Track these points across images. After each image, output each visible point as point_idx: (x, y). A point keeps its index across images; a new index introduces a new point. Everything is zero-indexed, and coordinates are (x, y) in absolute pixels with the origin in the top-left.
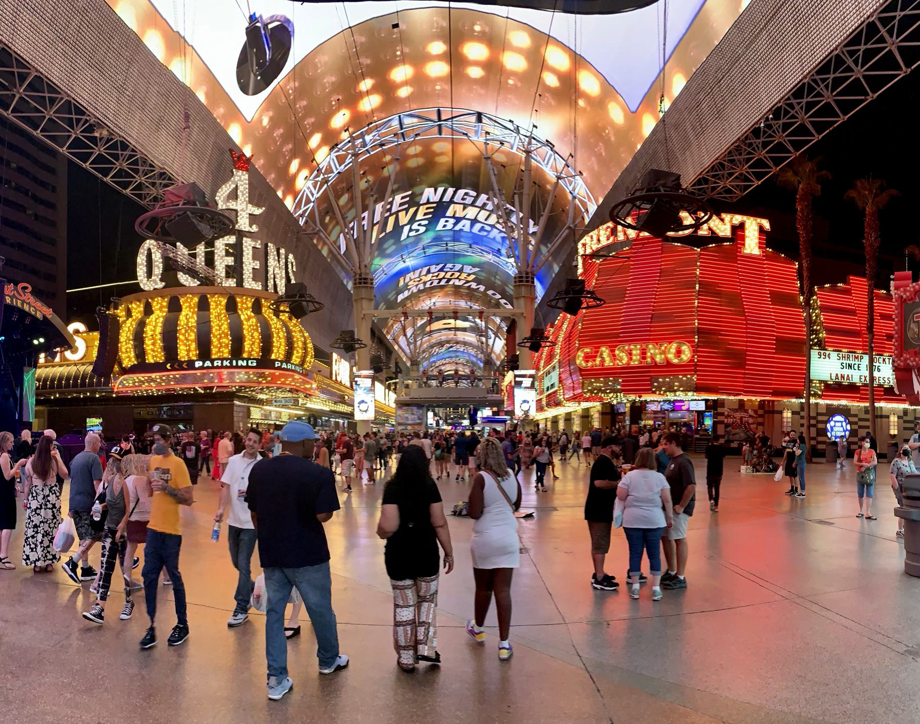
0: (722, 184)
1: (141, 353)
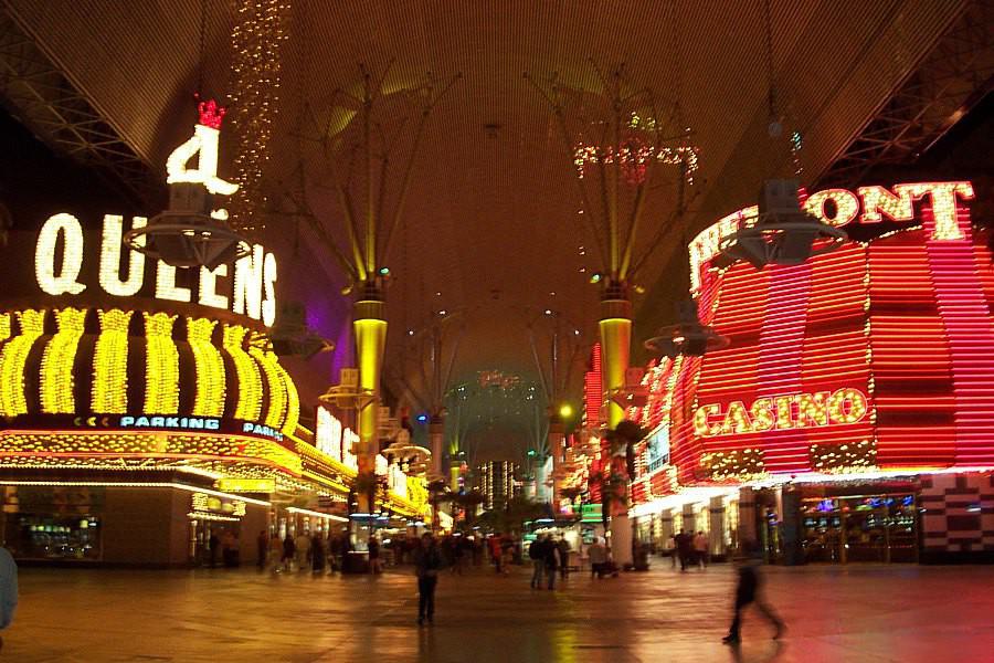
0: (888, 144)
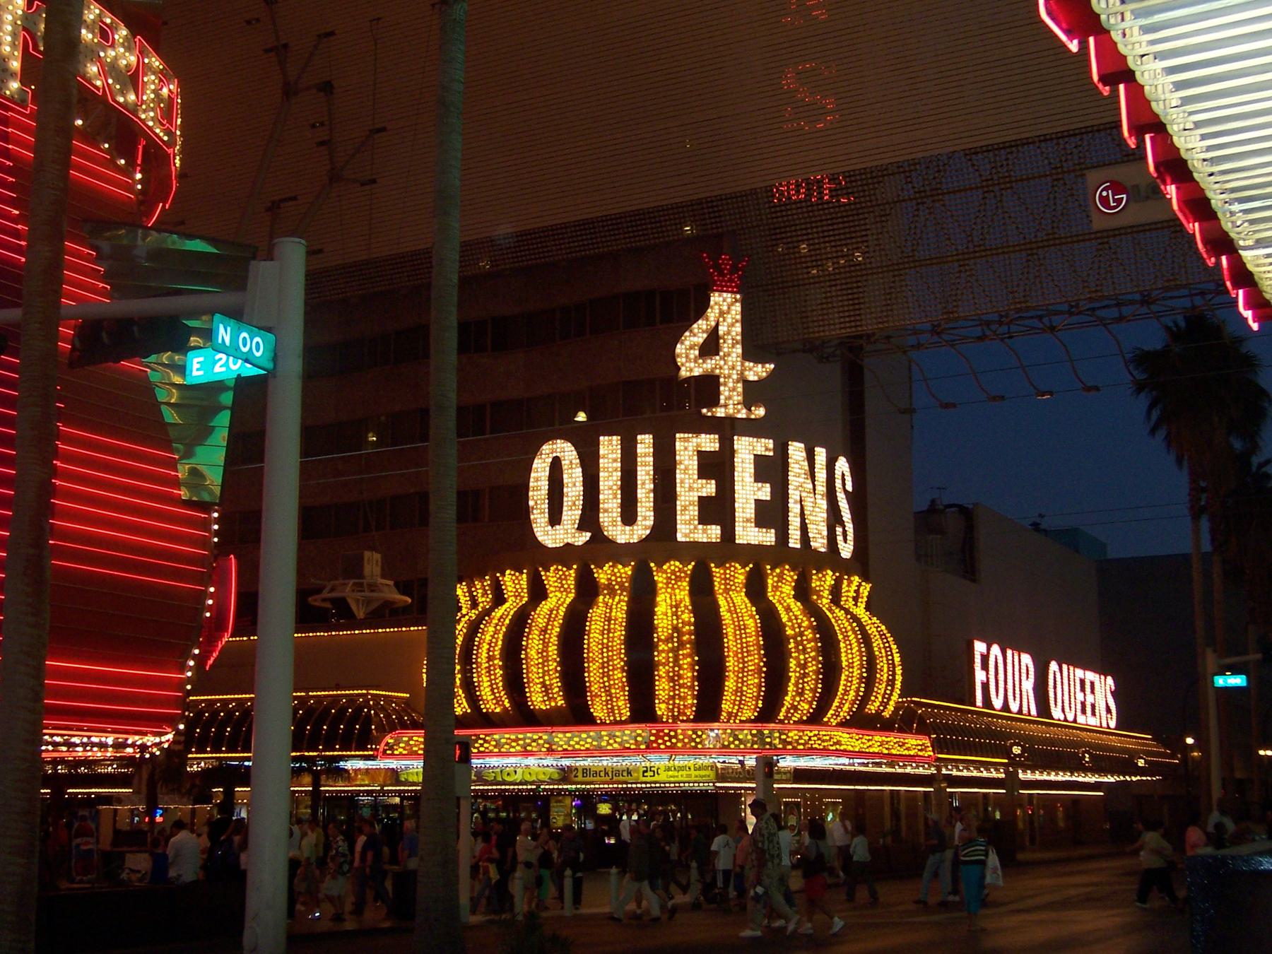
1: (515, 682)
